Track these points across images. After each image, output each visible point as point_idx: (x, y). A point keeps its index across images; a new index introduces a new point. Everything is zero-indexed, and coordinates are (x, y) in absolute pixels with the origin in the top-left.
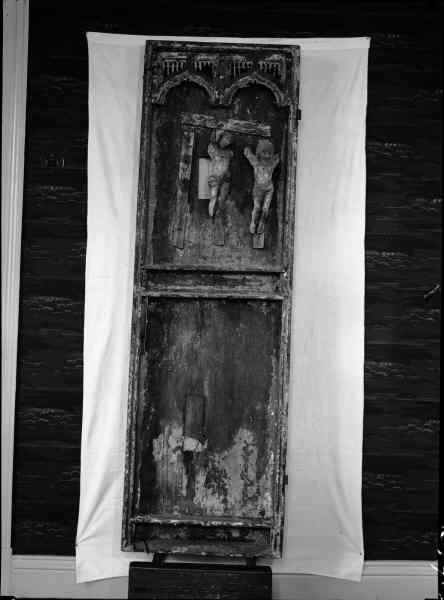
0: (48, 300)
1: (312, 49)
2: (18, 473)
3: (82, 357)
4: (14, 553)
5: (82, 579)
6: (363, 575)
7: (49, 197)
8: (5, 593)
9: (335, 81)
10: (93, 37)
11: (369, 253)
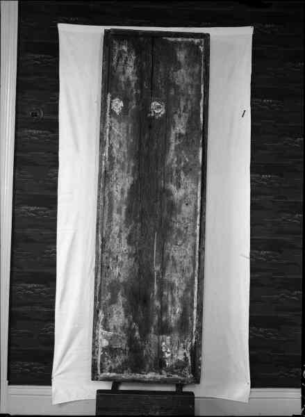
0: (30, 286)
1: (218, 34)
2: (15, 251)
3: (56, 248)
4: (9, 384)
5: (56, 402)
6: (249, 399)
7: (32, 138)
8: (4, 412)
9: (232, 50)
10: (62, 27)
11: (253, 175)
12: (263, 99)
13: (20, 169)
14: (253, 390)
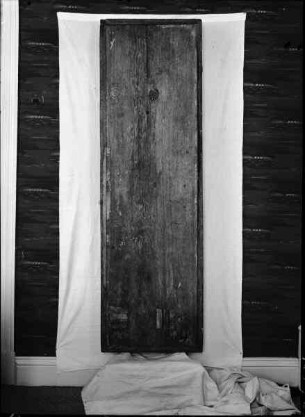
1: (209, 20)
9: (225, 34)
10: (61, 16)
13: (24, 153)
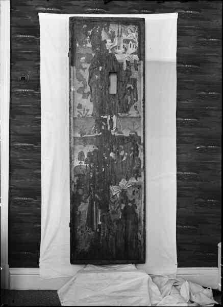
1: (150, 19)
9: (163, 30)
12: (185, 65)
13: (14, 117)
14: (179, 268)
